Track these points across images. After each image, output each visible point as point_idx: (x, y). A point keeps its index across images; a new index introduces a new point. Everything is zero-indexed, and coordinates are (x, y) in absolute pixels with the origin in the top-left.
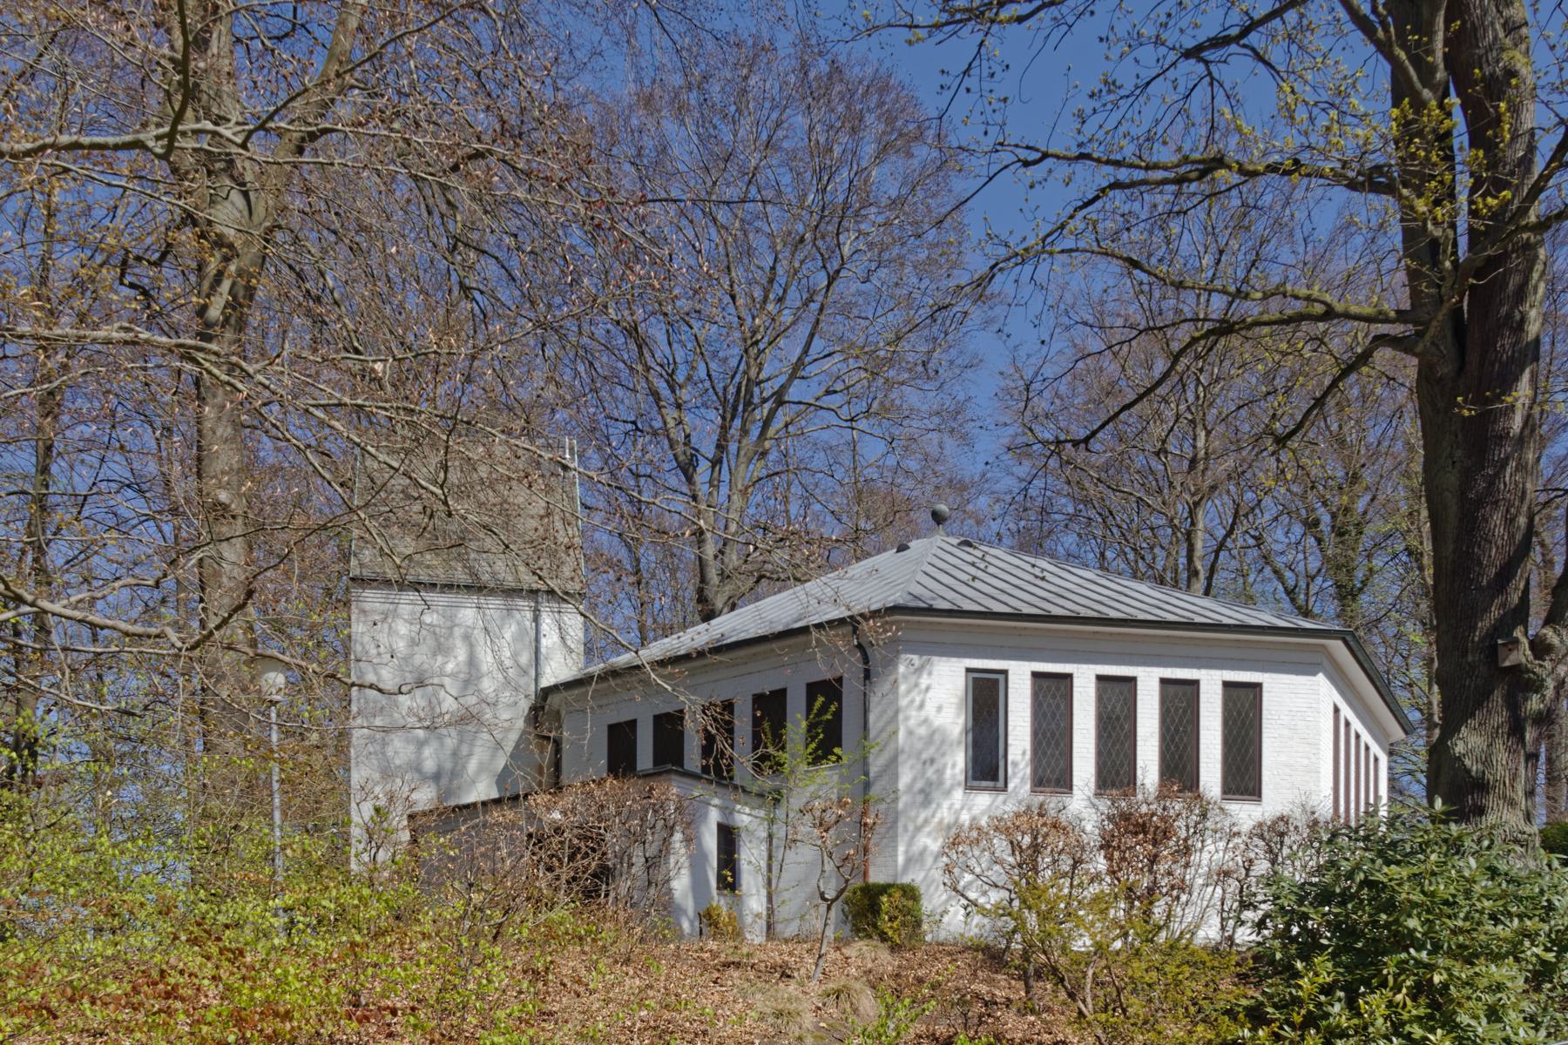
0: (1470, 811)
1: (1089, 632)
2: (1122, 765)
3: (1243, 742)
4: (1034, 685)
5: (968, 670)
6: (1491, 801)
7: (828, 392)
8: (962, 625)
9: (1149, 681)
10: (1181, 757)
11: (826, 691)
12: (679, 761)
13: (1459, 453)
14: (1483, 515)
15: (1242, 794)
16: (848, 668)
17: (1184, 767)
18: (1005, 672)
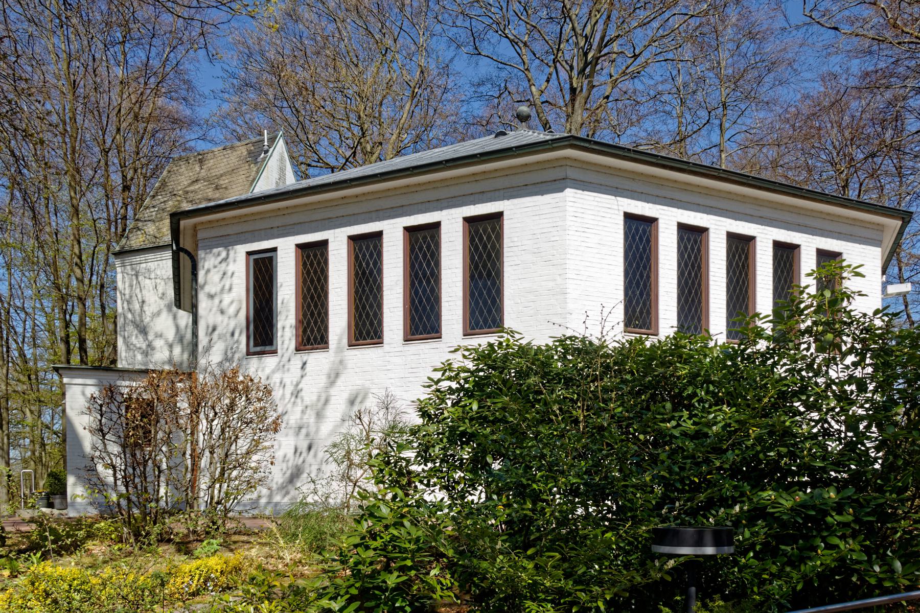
5: (249, 254)
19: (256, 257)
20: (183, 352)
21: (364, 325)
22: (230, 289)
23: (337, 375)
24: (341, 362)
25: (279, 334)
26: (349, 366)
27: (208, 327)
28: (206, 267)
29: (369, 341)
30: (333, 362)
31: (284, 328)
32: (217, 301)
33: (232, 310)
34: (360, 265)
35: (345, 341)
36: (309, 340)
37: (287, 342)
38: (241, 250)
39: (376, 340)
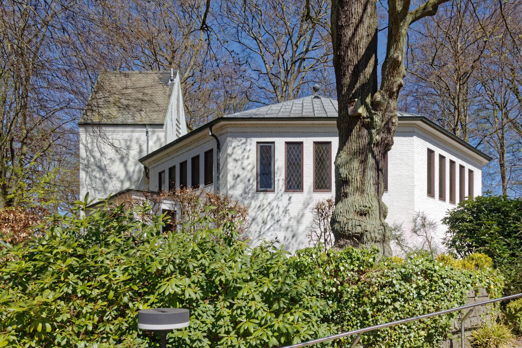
5: (258, 143)
8: (254, 124)
11: (209, 154)
14: (344, 34)
15: (320, 189)
18: (273, 143)
24: (311, 198)
25: (276, 183)
27: (234, 176)
29: (322, 190)
30: (306, 198)
31: (279, 180)
33: (249, 168)
35: (312, 189)
37: (280, 187)
38: (255, 140)
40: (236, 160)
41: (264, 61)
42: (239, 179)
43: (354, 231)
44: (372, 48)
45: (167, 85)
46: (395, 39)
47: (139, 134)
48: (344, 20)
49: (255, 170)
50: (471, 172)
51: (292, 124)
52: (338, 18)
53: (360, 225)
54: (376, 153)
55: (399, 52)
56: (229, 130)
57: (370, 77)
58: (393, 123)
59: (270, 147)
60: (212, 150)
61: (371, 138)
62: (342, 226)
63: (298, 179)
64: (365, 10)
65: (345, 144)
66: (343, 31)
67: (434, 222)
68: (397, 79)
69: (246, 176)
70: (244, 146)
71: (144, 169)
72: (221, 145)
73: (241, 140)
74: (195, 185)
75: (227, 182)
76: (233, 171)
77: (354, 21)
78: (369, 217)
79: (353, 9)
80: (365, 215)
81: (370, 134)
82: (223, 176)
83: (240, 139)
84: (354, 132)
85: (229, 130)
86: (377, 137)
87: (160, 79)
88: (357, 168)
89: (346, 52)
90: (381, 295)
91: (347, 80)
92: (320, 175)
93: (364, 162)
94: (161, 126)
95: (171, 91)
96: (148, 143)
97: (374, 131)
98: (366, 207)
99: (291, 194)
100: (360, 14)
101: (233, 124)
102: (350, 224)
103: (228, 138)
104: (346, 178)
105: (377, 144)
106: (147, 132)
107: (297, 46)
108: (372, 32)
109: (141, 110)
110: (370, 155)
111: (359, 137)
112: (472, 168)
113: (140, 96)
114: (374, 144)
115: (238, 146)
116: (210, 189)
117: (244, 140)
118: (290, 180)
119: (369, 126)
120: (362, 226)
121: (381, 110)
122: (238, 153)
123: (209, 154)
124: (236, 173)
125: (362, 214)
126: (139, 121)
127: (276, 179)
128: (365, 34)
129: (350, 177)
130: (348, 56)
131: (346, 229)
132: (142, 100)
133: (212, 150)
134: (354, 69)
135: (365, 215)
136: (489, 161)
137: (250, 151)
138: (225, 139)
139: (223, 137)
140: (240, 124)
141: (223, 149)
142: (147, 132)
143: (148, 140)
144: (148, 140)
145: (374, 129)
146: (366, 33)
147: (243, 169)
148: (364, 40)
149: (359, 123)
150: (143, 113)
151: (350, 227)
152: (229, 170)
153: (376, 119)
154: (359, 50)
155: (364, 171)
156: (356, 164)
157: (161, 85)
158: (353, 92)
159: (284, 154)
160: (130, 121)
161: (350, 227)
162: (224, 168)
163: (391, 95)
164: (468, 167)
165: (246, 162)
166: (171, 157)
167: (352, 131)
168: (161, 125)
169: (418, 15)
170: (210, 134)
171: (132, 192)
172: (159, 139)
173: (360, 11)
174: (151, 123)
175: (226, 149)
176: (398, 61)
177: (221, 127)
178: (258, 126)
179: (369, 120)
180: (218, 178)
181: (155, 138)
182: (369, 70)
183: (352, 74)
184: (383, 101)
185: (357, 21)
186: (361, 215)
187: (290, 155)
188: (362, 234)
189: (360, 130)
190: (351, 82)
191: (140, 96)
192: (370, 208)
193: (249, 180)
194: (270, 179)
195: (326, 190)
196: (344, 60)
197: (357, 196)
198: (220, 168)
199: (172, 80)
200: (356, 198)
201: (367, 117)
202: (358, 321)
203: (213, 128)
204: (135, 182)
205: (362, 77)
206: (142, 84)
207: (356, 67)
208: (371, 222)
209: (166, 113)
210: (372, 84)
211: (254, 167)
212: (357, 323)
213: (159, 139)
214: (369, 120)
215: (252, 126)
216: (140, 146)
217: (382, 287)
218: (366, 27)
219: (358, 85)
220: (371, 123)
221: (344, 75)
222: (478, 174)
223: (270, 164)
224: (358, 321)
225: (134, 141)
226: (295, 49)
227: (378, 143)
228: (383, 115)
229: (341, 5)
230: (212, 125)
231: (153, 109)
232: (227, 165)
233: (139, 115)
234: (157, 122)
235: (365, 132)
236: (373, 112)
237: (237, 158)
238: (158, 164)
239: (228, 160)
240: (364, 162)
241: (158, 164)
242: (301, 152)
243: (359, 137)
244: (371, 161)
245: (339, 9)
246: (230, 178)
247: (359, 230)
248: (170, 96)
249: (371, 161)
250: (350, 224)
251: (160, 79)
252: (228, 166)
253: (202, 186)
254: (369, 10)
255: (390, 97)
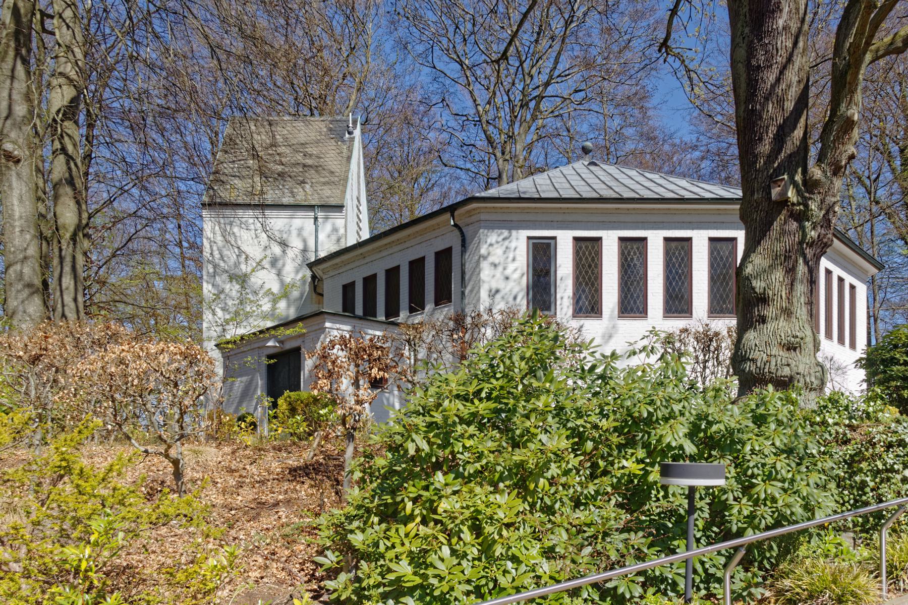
0: (756, 321)
1: (613, 209)
2: (638, 297)
3: (724, 278)
4: (620, 247)
5: (529, 238)
6: (770, 311)
7: (576, 91)
8: (524, 208)
9: (656, 240)
10: (680, 290)
11: (444, 257)
12: (353, 312)
13: (747, 30)
14: (762, 78)
15: (680, 313)
16: (452, 240)
17: (682, 297)
18: (554, 238)
19: (535, 241)
20: (289, 306)
21: (629, 303)
22: (514, 260)
23: (610, 337)
24: (614, 327)
25: (558, 303)
26: (620, 332)
27: (490, 291)
28: (489, 241)
29: (632, 315)
30: (607, 328)
31: (562, 298)
32: (500, 269)
33: (516, 276)
34: (626, 259)
35: (616, 312)
36: (581, 309)
37: (565, 310)
38: (525, 234)
39: (643, 315)
40: (495, 265)
41: (475, 101)
42: (498, 296)
43: (779, 374)
44: (802, 102)
45: (344, 141)
46: (850, 88)
47: (303, 222)
48: (763, 58)
49: (524, 281)
50: (852, 287)
51: (585, 209)
52: (752, 53)
53: (788, 365)
54: (809, 256)
55: (854, 107)
56: (483, 217)
57: (801, 143)
58: (835, 212)
59: (549, 245)
60: (449, 250)
61: (804, 235)
62: (759, 365)
63: (593, 296)
64: (795, 44)
65: (759, 243)
66: (761, 74)
67: (844, 364)
68: (847, 147)
69: (511, 291)
70: (506, 243)
71: (310, 279)
72: (467, 241)
73: (501, 233)
74: (417, 305)
75: (479, 300)
76: (489, 282)
77: (779, 59)
78: (800, 352)
79: (779, 43)
80: (795, 349)
81: (802, 228)
82: (471, 291)
83: (499, 231)
84: (776, 225)
85: (483, 217)
86: (813, 233)
87: (330, 130)
88: (781, 279)
89: (763, 106)
90: (890, 459)
91: (765, 147)
92: (629, 290)
93: (791, 271)
94: (338, 209)
95: (350, 150)
96: (316, 237)
97: (808, 224)
98: (797, 337)
99: (583, 321)
100: (790, 50)
101: (490, 208)
102: (773, 363)
103: (481, 231)
104: (764, 294)
105: (811, 245)
106: (316, 219)
107: (532, 77)
108: (803, 75)
109: (303, 182)
110: (801, 261)
111: (783, 233)
112: (855, 282)
113: (300, 158)
114: (807, 244)
115: (497, 242)
116: (445, 313)
117: (506, 233)
118: (580, 298)
119: (801, 217)
120: (792, 366)
121: (819, 193)
122: (497, 254)
123: (444, 257)
124: (494, 286)
125: (791, 347)
126: (302, 200)
127: (558, 296)
128: (795, 79)
129: (771, 293)
130: (768, 111)
131: (766, 370)
132: (304, 166)
133: (449, 250)
134: (778, 131)
135: (795, 349)
136: (879, 270)
137: (515, 249)
138: (476, 232)
139: (471, 228)
140: (501, 208)
141: (471, 247)
142: (316, 219)
143: (316, 231)
144: (316, 231)
145: (808, 221)
146: (797, 78)
147: (507, 278)
148: (794, 89)
149: (784, 212)
150: (307, 186)
151: (773, 367)
152: (484, 282)
153: (813, 206)
154: (786, 103)
155: (792, 285)
156: (779, 275)
157: (332, 141)
158: (776, 165)
159: (571, 257)
160: (286, 200)
161: (773, 367)
162: (474, 278)
163: (837, 170)
164: (849, 279)
165: (511, 267)
166: (368, 260)
167: (772, 224)
168: (339, 207)
169: (880, 53)
170: (452, 223)
171: (326, 316)
172: (335, 230)
173: (789, 44)
174: (323, 203)
175: (478, 247)
176: (853, 121)
177: (469, 211)
178: (570, 211)
179: (802, 207)
180: (463, 293)
181: (328, 227)
182: (798, 133)
183: (774, 138)
184: (823, 179)
185: (784, 60)
186: (788, 349)
187: (581, 259)
188: (791, 379)
189: (785, 223)
190: (772, 150)
191: (299, 157)
192: (802, 339)
193: (515, 298)
194: (549, 294)
195: (638, 315)
196: (761, 118)
197: (782, 323)
198: (467, 277)
199: (350, 133)
200: (781, 324)
201: (799, 204)
202: (852, 496)
203: (456, 213)
204: (296, 300)
205: (789, 143)
206: (302, 138)
207: (781, 128)
208: (804, 360)
209: (345, 187)
210: (802, 154)
211: (523, 275)
212: (850, 499)
213: (335, 230)
214: (802, 207)
215: (518, 211)
216: (305, 241)
217: (889, 446)
218: (796, 69)
219: (783, 155)
220: (804, 212)
221: (761, 139)
222: (862, 291)
223: (548, 273)
224: (852, 496)
225: (294, 233)
226: (528, 82)
227: (813, 242)
228: (822, 201)
229: (757, 36)
230: (455, 209)
231: (322, 180)
232: (479, 274)
233: (301, 190)
234: (332, 201)
235: (794, 225)
236: (807, 195)
237: (497, 262)
238: (341, 271)
239: (482, 265)
240: (791, 271)
241: (341, 271)
242: (598, 254)
243: (783, 233)
244: (802, 269)
245: (752, 42)
246: (484, 294)
247: (786, 371)
248: (349, 158)
249: (802, 269)
250: (773, 363)
251: (330, 130)
252: (482, 275)
253: (429, 307)
254: (801, 44)
255: (835, 174)
